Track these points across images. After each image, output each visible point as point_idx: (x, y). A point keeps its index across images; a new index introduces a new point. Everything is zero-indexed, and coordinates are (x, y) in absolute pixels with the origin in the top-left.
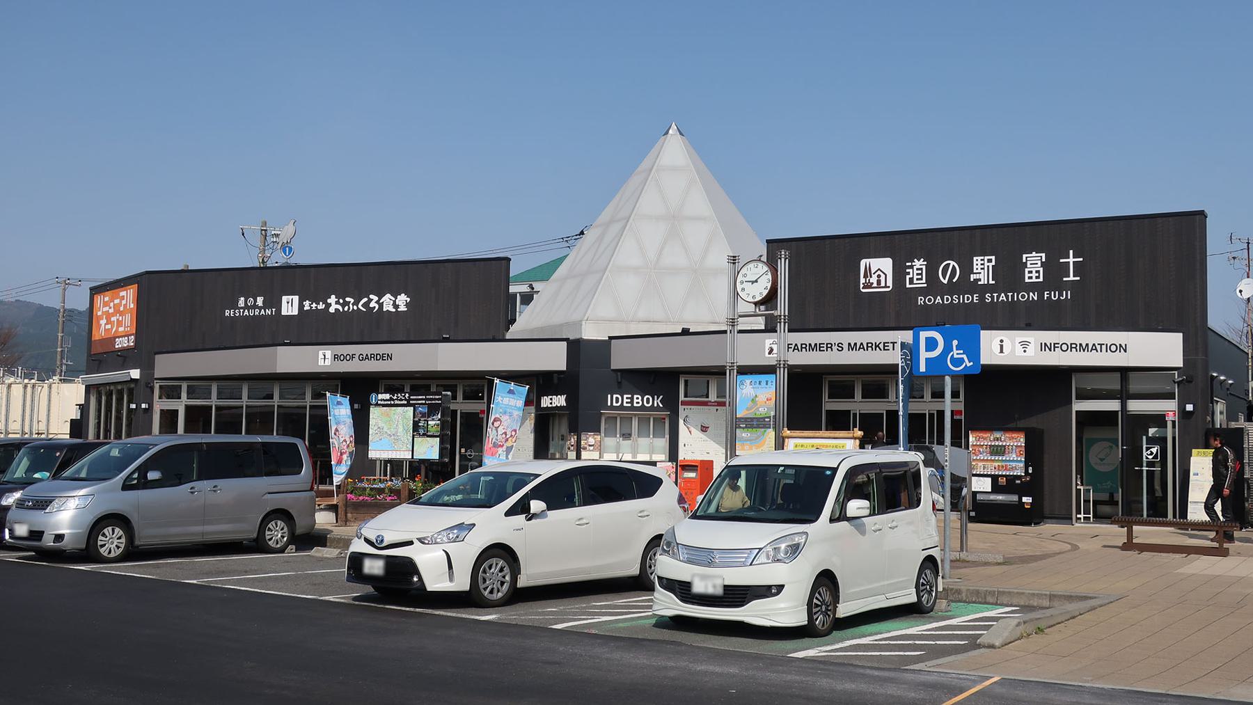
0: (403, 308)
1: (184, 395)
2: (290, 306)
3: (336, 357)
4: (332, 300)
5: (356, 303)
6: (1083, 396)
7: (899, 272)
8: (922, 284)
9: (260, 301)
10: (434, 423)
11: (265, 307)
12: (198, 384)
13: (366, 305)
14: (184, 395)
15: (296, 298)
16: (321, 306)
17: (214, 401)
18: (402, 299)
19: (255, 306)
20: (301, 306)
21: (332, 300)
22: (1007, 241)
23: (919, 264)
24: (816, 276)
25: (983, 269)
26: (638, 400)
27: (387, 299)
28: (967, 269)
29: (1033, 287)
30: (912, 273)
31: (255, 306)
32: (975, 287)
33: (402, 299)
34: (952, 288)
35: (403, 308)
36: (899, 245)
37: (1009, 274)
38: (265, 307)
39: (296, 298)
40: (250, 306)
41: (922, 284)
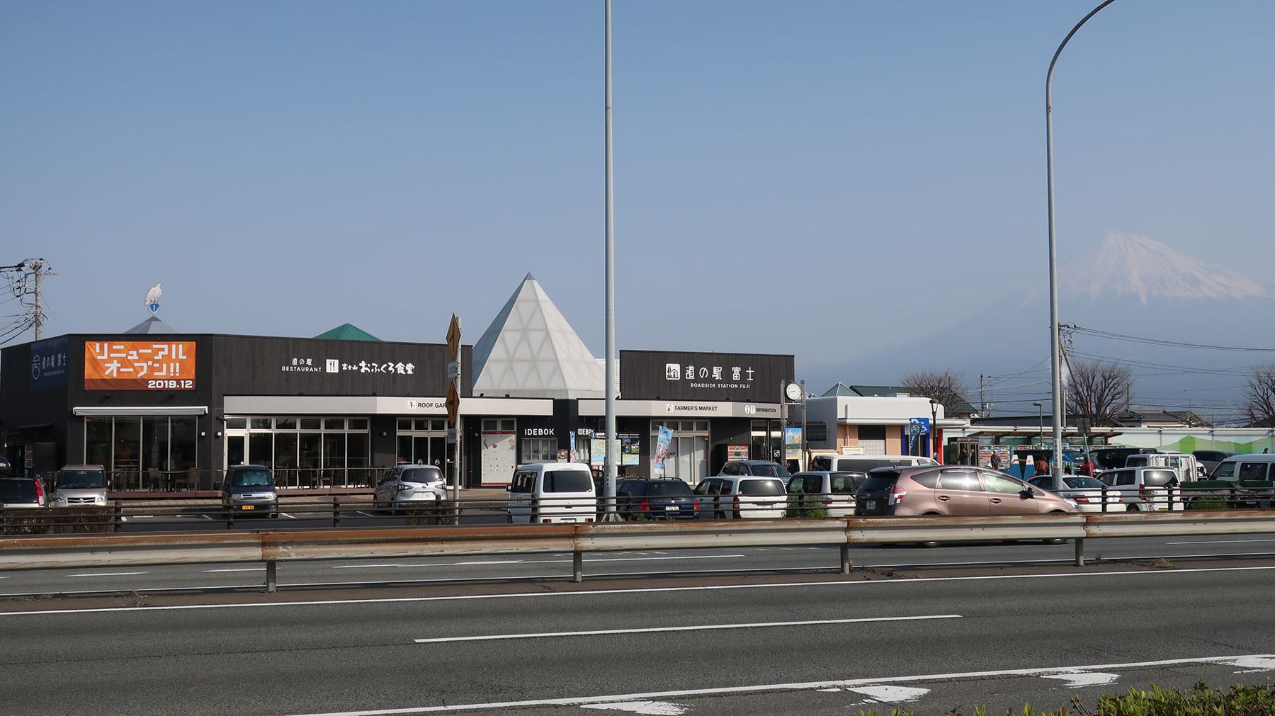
0: (410, 372)
1: (248, 425)
2: (332, 366)
3: (420, 405)
4: (363, 364)
5: (379, 367)
6: (755, 429)
7: (683, 371)
8: (692, 377)
9: (309, 362)
10: (635, 447)
11: (313, 366)
12: (262, 420)
13: (386, 369)
14: (248, 425)
15: (337, 362)
16: (355, 368)
17: (346, 430)
18: (410, 367)
19: (305, 365)
20: (340, 367)
21: (363, 364)
22: (727, 360)
23: (691, 368)
24: (641, 371)
25: (717, 372)
26: (541, 432)
27: (400, 366)
28: (711, 372)
29: (736, 382)
30: (689, 372)
31: (305, 365)
32: (714, 381)
33: (410, 367)
34: (705, 381)
35: (410, 372)
36: (683, 358)
37: (727, 375)
38: (313, 366)
39: (337, 362)
40: (301, 365)
41: (692, 377)
